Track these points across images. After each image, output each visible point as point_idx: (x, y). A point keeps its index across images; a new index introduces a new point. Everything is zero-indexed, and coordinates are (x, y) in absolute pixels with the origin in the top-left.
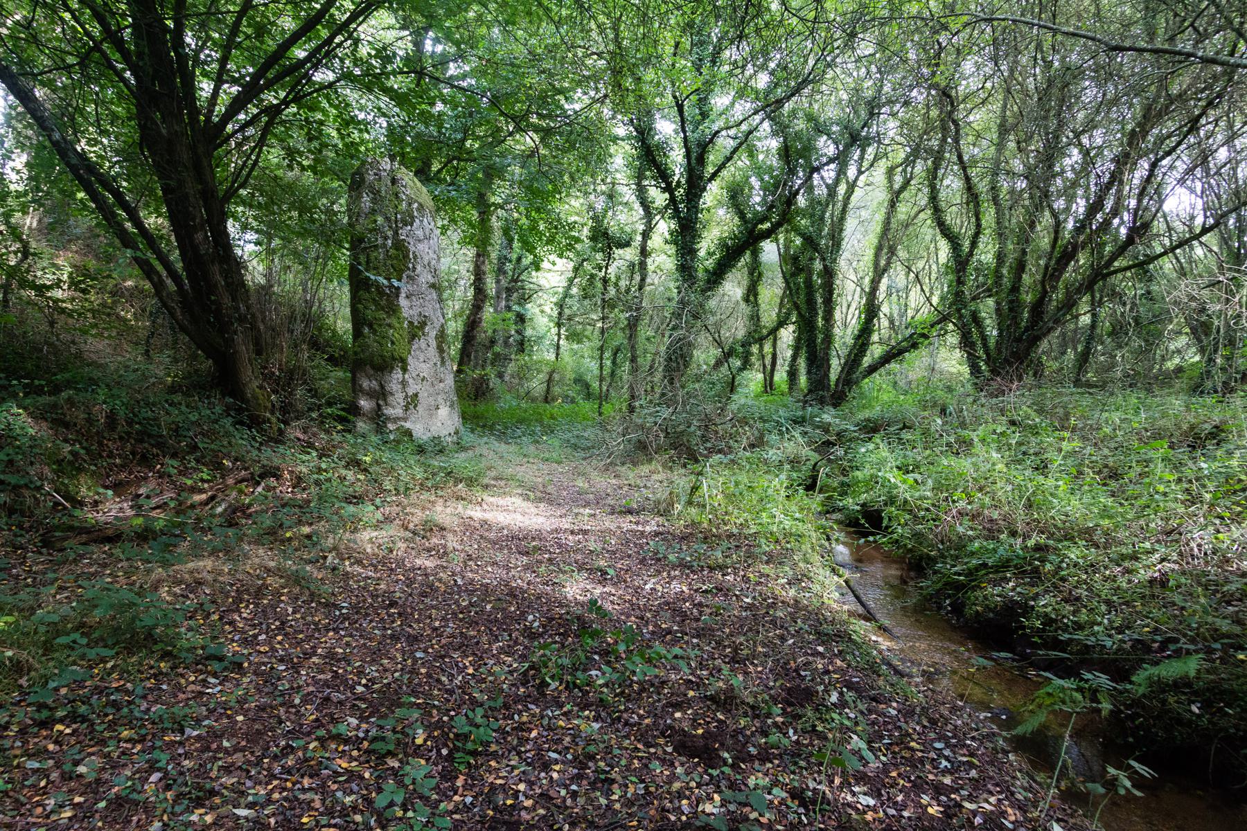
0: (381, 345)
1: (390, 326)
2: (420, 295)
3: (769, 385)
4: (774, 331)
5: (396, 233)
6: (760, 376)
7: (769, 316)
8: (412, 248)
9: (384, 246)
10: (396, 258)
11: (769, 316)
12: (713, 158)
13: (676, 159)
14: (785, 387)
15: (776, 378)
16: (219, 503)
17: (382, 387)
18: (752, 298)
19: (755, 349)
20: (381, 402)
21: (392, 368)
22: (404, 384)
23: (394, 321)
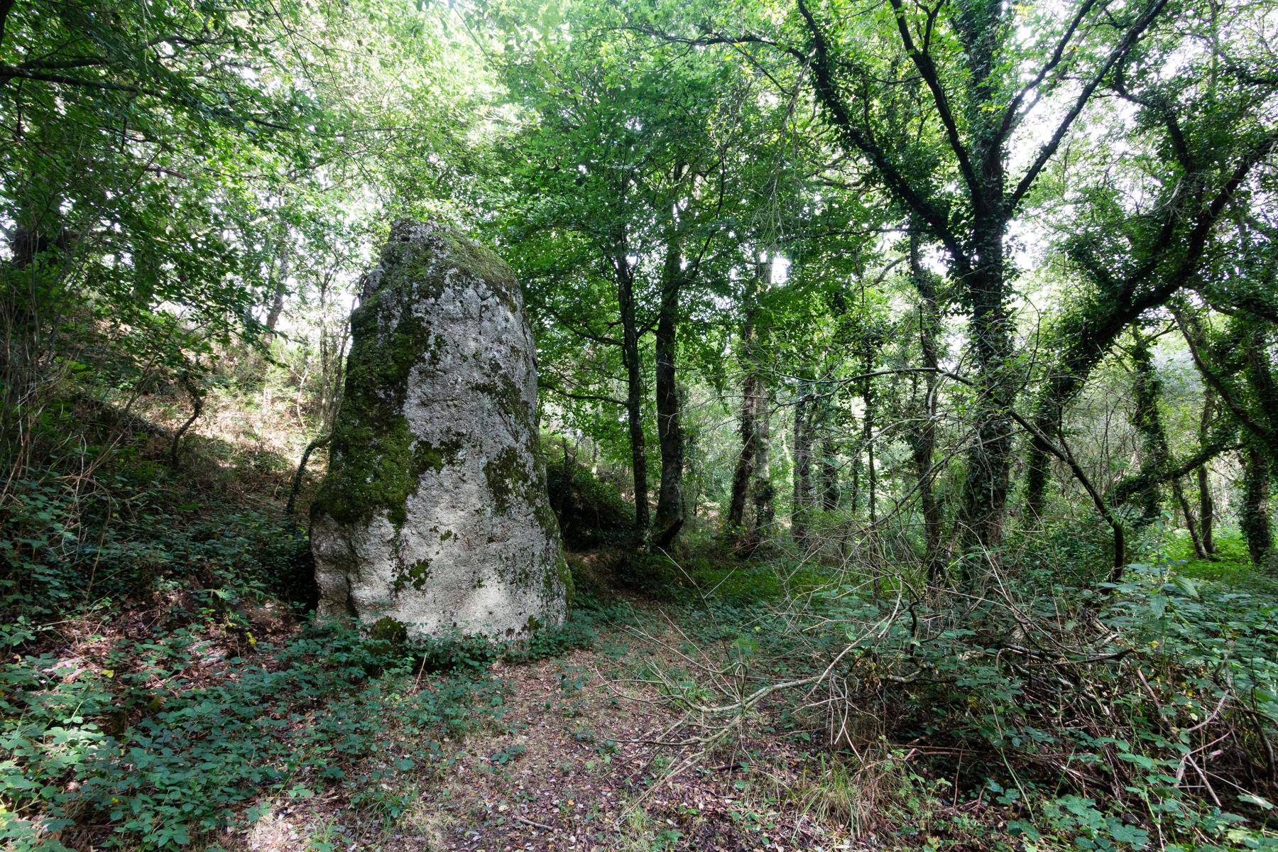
0: (354, 479)
1: (379, 449)
2: (450, 400)
3: (1203, 546)
4: (1198, 463)
5: (408, 309)
6: (1182, 533)
7: (1182, 444)
8: (435, 331)
9: (387, 328)
10: (403, 344)
11: (1182, 444)
12: (1018, 156)
13: (949, 185)
14: (1240, 548)
15: (1216, 533)
16: (1240, 620)
17: (352, 550)
18: (1146, 419)
19: (1166, 490)
20: (352, 577)
21: (369, 519)
22: (396, 545)
23: (389, 442)
